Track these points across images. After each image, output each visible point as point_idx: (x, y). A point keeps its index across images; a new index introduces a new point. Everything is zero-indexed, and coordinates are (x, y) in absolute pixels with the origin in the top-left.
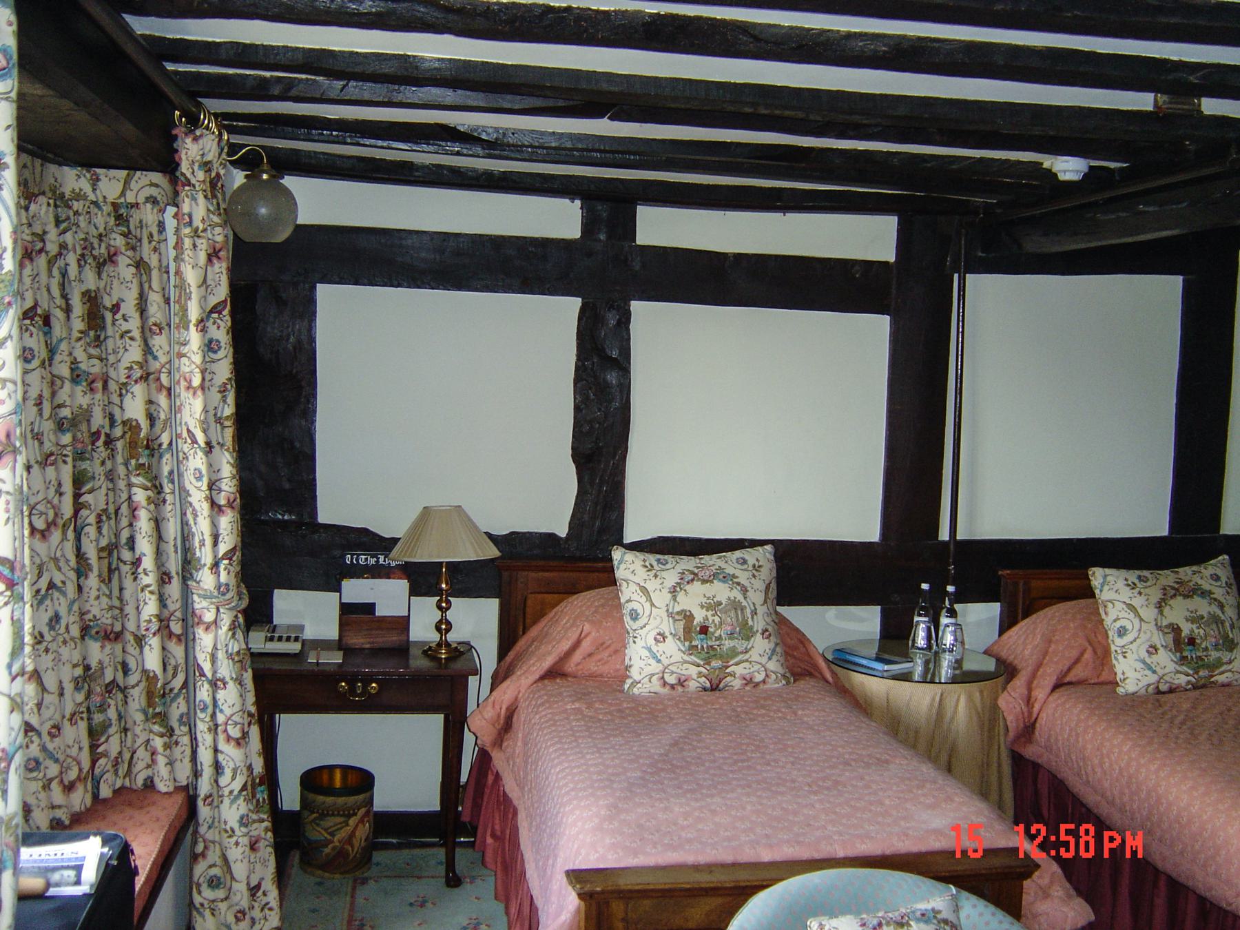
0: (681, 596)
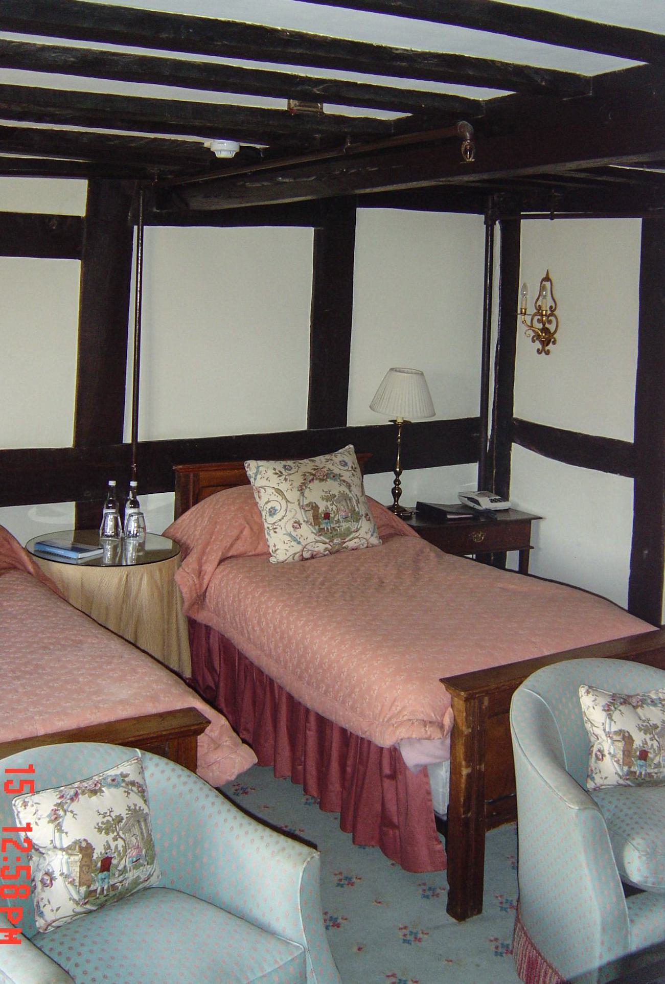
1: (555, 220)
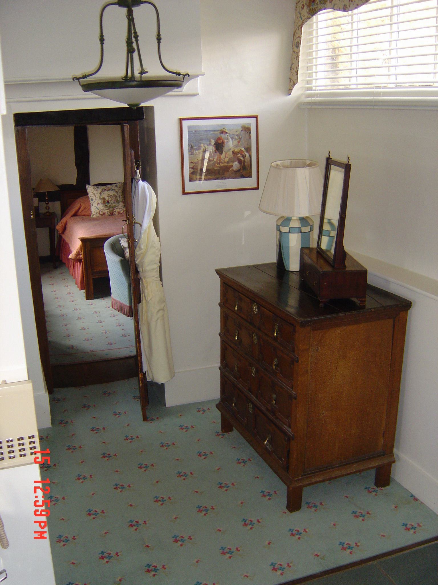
0: (102, 194)
1: (137, 31)
